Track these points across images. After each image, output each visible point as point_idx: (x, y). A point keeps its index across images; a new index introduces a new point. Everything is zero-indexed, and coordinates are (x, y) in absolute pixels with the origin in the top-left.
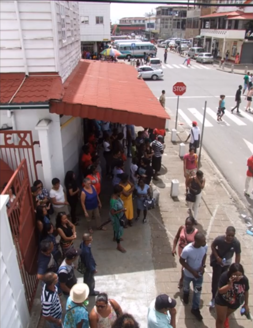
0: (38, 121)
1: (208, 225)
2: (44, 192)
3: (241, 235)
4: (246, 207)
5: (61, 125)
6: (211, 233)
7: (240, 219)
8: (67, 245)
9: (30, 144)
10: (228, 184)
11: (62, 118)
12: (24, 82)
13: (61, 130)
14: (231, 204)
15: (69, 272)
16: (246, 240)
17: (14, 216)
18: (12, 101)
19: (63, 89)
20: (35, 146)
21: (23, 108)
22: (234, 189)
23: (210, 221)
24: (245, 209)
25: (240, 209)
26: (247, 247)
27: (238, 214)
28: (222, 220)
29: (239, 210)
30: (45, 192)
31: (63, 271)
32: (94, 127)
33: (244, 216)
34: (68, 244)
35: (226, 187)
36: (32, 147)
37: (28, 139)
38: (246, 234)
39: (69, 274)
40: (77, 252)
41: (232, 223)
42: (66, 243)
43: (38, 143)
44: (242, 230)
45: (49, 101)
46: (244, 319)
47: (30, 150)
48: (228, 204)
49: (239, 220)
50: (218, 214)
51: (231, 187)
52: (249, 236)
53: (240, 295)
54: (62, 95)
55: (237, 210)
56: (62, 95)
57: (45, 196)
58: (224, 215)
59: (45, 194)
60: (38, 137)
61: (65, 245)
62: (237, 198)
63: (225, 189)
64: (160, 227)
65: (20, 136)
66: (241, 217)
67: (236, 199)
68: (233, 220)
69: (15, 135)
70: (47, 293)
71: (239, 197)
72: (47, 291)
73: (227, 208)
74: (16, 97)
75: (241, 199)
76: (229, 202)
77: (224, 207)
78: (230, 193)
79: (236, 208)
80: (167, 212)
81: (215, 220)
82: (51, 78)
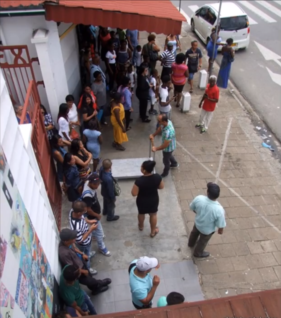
0: (31, 32)
1: (224, 140)
2: (47, 118)
3: (257, 148)
4: (261, 119)
5: (60, 36)
6: (228, 148)
7: (255, 132)
8: (83, 174)
9: (28, 62)
10: (240, 94)
11: (60, 26)
13: (60, 42)
14: (245, 117)
16: (262, 153)
17: (34, 141)
20: (34, 64)
22: (247, 100)
23: (225, 136)
24: (259, 121)
25: (254, 121)
26: (264, 160)
27: (253, 127)
28: (237, 134)
29: (253, 122)
30: (49, 118)
31: (88, 195)
32: (123, 98)
33: (259, 128)
34: (85, 173)
35: (238, 98)
36: (30, 65)
37: (24, 55)
38: (262, 147)
39: (93, 197)
40: (95, 179)
41: (247, 136)
42: (82, 173)
43: (36, 59)
44: (258, 142)
45: (43, 4)
46: (264, 227)
47: (28, 69)
48: (242, 116)
49: (254, 133)
50: (233, 128)
51: (244, 98)
52: (265, 148)
55: (251, 123)
57: (49, 123)
58: (240, 128)
59: (49, 120)
60: (36, 53)
61: (82, 174)
62: (250, 109)
63: (238, 101)
65: (13, 53)
66: (256, 130)
67: (249, 111)
68: (248, 133)
69: (7, 52)
70: (74, 222)
71: (252, 108)
72: (74, 220)
73: (241, 120)
75: (254, 111)
76: (243, 115)
77: (238, 120)
78: (243, 105)
79: (250, 121)
80: (180, 128)
81: (230, 134)
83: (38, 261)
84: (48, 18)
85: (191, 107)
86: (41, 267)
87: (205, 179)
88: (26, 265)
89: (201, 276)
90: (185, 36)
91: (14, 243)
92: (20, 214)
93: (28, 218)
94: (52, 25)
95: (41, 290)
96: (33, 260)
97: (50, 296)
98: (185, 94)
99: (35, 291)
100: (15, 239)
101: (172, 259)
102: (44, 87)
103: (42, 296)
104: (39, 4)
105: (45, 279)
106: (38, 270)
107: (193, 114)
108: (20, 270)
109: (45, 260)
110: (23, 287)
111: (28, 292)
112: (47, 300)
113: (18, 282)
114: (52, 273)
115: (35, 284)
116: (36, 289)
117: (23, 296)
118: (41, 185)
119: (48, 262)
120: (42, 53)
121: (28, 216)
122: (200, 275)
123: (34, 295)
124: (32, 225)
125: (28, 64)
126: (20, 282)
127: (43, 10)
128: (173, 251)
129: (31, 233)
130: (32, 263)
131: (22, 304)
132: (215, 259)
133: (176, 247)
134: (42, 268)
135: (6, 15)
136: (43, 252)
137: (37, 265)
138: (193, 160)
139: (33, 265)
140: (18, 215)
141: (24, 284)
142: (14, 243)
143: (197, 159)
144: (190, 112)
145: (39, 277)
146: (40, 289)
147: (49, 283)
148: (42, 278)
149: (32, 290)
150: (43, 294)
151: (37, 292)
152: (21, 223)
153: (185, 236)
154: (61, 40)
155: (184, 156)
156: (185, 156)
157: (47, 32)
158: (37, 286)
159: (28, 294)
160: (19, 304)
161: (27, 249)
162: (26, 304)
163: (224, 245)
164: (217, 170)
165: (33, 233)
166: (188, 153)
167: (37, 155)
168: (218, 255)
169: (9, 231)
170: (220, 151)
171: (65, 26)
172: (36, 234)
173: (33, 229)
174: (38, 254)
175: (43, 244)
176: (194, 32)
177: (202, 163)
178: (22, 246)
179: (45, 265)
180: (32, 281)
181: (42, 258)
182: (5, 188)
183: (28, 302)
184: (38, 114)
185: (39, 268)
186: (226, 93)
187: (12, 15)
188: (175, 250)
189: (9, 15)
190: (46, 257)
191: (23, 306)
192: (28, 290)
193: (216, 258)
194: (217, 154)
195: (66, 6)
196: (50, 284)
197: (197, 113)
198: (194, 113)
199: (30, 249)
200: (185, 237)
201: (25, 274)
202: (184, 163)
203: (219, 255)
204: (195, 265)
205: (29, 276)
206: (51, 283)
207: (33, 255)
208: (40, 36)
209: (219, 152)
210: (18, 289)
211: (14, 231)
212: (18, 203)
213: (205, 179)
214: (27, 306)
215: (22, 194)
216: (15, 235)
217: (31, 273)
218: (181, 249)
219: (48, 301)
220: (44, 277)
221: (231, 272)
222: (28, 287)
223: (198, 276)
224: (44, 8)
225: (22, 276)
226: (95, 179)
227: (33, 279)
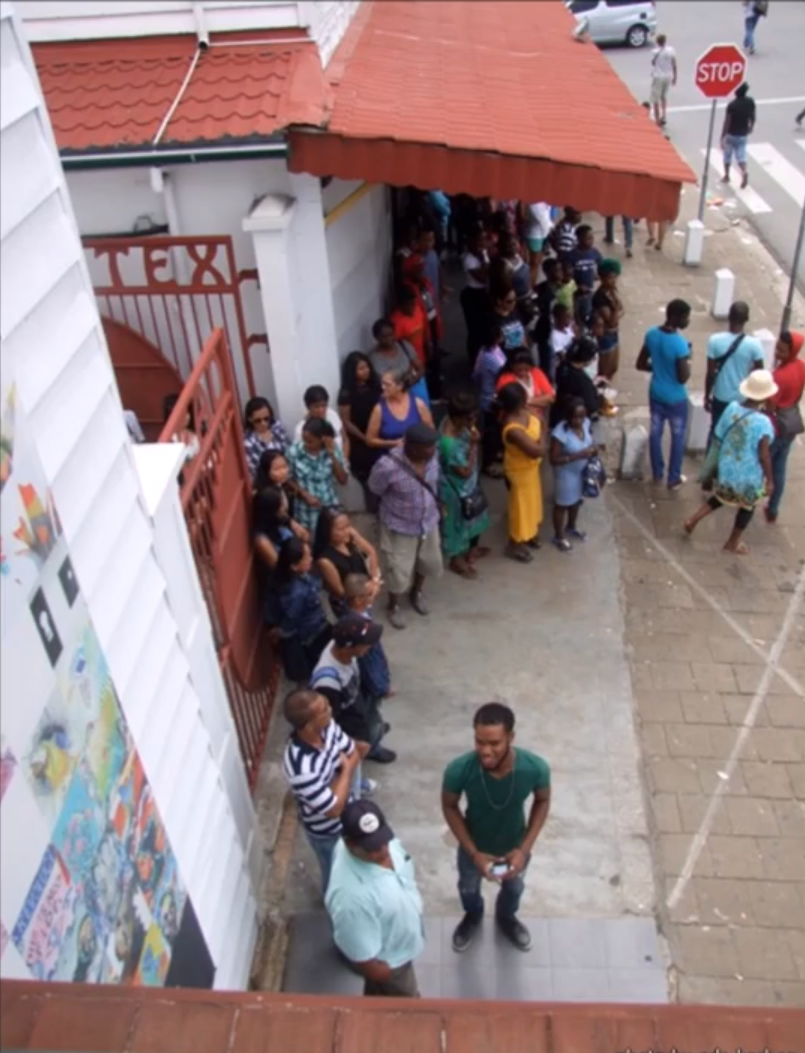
5: (325, 215)
9: (228, 280)
12: (197, 66)
13: (326, 229)
18: (162, 138)
19: (328, 87)
20: (245, 286)
21: (201, 158)
36: (234, 289)
37: (220, 261)
40: (364, 632)
43: (252, 274)
47: (229, 298)
54: (325, 108)
56: (325, 108)
60: (252, 257)
65: (194, 255)
69: (180, 251)
82: (287, 50)
83: (131, 839)
84: (295, 166)
86: (140, 859)
87: (731, 663)
88: (79, 843)
89: (677, 978)
90: (722, 231)
91: (45, 766)
92: (85, 687)
93: (116, 704)
94: (307, 186)
95: (125, 928)
96: (109, 830)
97: (156, 954)
99: (100, 927)
100: (49, 755)
101: (590, 905)
102: (268, 350)
103: (123, 949)
105: (149, 901)
106: (124, 864)
108: (52, 853)
109: (158, 842)
110: (52, 901)
111: (68, 922)
112: (141, 965)
113: (34, 883)
114: (180, 887)
115: (102, 903)
116: (103, 920)
117: (49, 931)
118: (198, 624)
119: (169, 850)
120: (270, 259)
121: (114, 700)
122: (673, 973)
123: (94, 938)
124: (126, 728)
125: (229, 287)
126: (43, 885)
128: (596, 880)
129: (115, 751)
130: (104, 841)
131: (39, 953)
132: (732, 926)
133: (607, 869)
134: (142, 863)
135: (185, 159)
136: (156, 814)
137: (123, 851)
138: (699, 600)
139: (105, 847)
141: (61, 894)
142: (45, 766)
143: (711, 600)
145: (126, 888)
146: (119, 924)
147: (163, 914)
148: (137, 892)
149: (89, 919)
150: (130, 941)
151: (106, 930)
152: (82, 714)
153: (642, 837)
156: (675, 587)
157: (289, 201)
158: (113, 912)
159: (70, 930)
160: (26, 952)
161: (92, 792)
162: (55, 956)
163: (770, 885)
164: (774, 640)
165: (126, 754)
166: (688, 577)
168: (743, 916)
169: (32, 726)
170: (793, 582)
171: (341, 187)
172: (137, 759)
173: (128, 741)
174: (134, 819)
175: (161, 793)
176: (65, 131)
177: (727, 612)
178: (72, 782)
179: (158, 857)
180: (94, 892)
181: (146, 834)
182: (39, 604)
183: (61, 951)
184: (228, 423)
185: (128, 858)
187: (201, 158)
188: (602, 878)
189: (193, 158)
190: (163, 831)
191: (38, 962)
192: (68, 917)
193: (735, 923)
194: (781, 590)
196: (166, 917)
199: (103, 798)
200: (639, 841)
201: (70, 867)
203: (747, 914)
204: (661, 936)
205: (83, 876)
206: (170, 917)
207: (112, 815)
208: (271, 213)
209: (788, 584)
210: (32, 904)
211: (53, 732)
212: (82, 657)
213: (731, 663)
214: (56, 964)
215: (104, 635)
216: (51, 744)
217: (93, 868)
218: (624, 878)
219: (148, 968)
220: (145, 891)
221: (783, 981)
222: (74, 910)
223: (668, 977)
225: (56, 870)
226: (364, 632)
227: (99, 887)
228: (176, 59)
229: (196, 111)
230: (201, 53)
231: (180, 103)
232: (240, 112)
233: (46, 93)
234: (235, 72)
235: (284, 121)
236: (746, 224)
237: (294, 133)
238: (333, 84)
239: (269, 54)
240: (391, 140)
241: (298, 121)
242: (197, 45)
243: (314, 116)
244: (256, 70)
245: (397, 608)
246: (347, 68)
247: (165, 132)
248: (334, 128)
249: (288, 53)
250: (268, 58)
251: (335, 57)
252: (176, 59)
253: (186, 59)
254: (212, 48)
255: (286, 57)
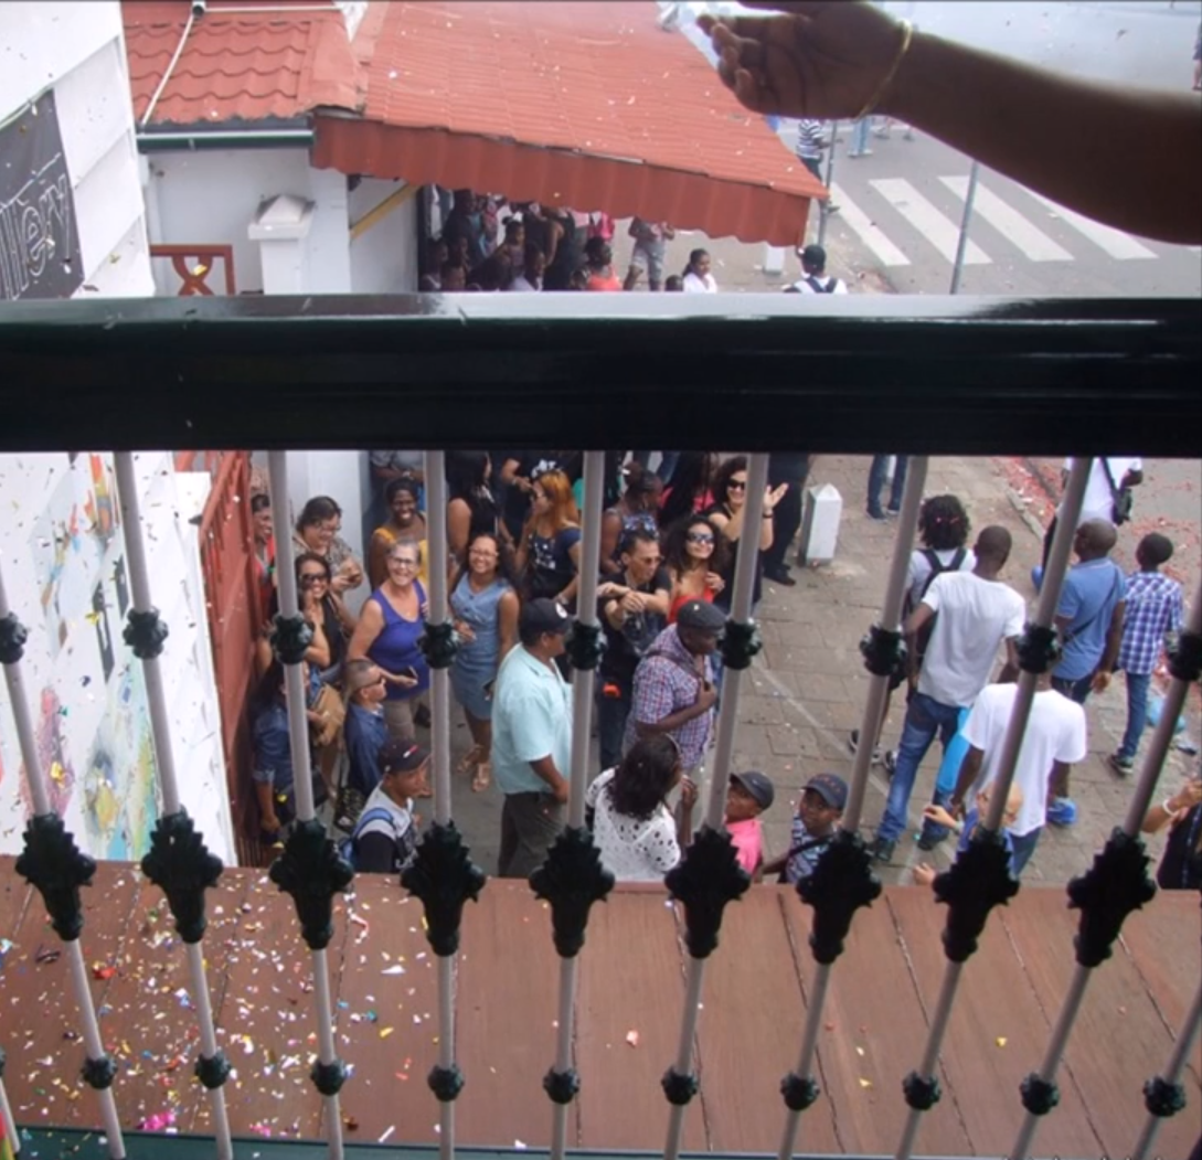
0: (255, 203)
11: (358, 189)
12: (190, 35)
13: (351, 244)
15: (401, 833)
18: (151, 118)
19: (360, 66)
21: (202, 145)
32: (465, 241)
40: (407, 754)
45: (311, 114)
53: (367, 728)
54: (359, 90)
56: (359, 90)
64: (759, 684)
65: (182, 270)
74: (169, 99)
80: (787, 621)
82: (305, 19)
85: (840, 549)
92: (129, 721)
94: (330, 186)
98: (819, 490)
104: (297, 114)
107: (850, 576)
127: (308, 133)
135: (182, 145)
140: (123, 724)
144: (834, 564)
154: (353, 238)
155: (789, 730)
156: (795, 731)
157: (307, 205)
167: (214, 615)
171: (376, 189)
184: (235, 475)
186: (999, 509)
187: (202, 145)
189: (192, 143)
195: (387, 122)
197: (864, 572)
198: (847, 569)
202: (787, 755)
208: (284, 217)
224: (309, 127)
226: (407, 754)
228: (163, 26)
229: (190, 87)
230: (195, 20)
231: (171, 78)
232: (251, 90)
233: (126, 28)
234: (236, 43)
235: (307, 102)
236: (876, 280)
237: (321, 117)
238: (363, 64)
239: (284, 23)
240: (446, 130)
241: (329, 103)
242: (191, 9)
243: (348, 98)
244: (266, 41)
245: (491, 618)
246: (376, 46)
247: (155, 111)
248: (370, 113)
249: (308, 23)
250: (283, 28)
251: (359, 33)
252: (163, 26)
253: (176, 25)
254: (209, 13)
255: (304, 27)
